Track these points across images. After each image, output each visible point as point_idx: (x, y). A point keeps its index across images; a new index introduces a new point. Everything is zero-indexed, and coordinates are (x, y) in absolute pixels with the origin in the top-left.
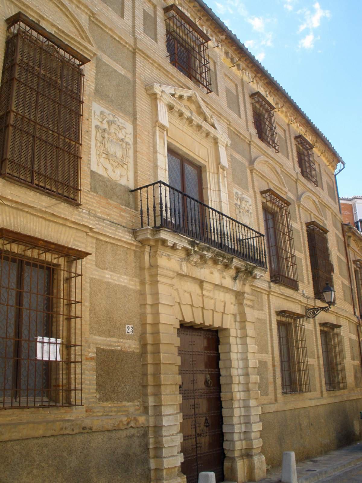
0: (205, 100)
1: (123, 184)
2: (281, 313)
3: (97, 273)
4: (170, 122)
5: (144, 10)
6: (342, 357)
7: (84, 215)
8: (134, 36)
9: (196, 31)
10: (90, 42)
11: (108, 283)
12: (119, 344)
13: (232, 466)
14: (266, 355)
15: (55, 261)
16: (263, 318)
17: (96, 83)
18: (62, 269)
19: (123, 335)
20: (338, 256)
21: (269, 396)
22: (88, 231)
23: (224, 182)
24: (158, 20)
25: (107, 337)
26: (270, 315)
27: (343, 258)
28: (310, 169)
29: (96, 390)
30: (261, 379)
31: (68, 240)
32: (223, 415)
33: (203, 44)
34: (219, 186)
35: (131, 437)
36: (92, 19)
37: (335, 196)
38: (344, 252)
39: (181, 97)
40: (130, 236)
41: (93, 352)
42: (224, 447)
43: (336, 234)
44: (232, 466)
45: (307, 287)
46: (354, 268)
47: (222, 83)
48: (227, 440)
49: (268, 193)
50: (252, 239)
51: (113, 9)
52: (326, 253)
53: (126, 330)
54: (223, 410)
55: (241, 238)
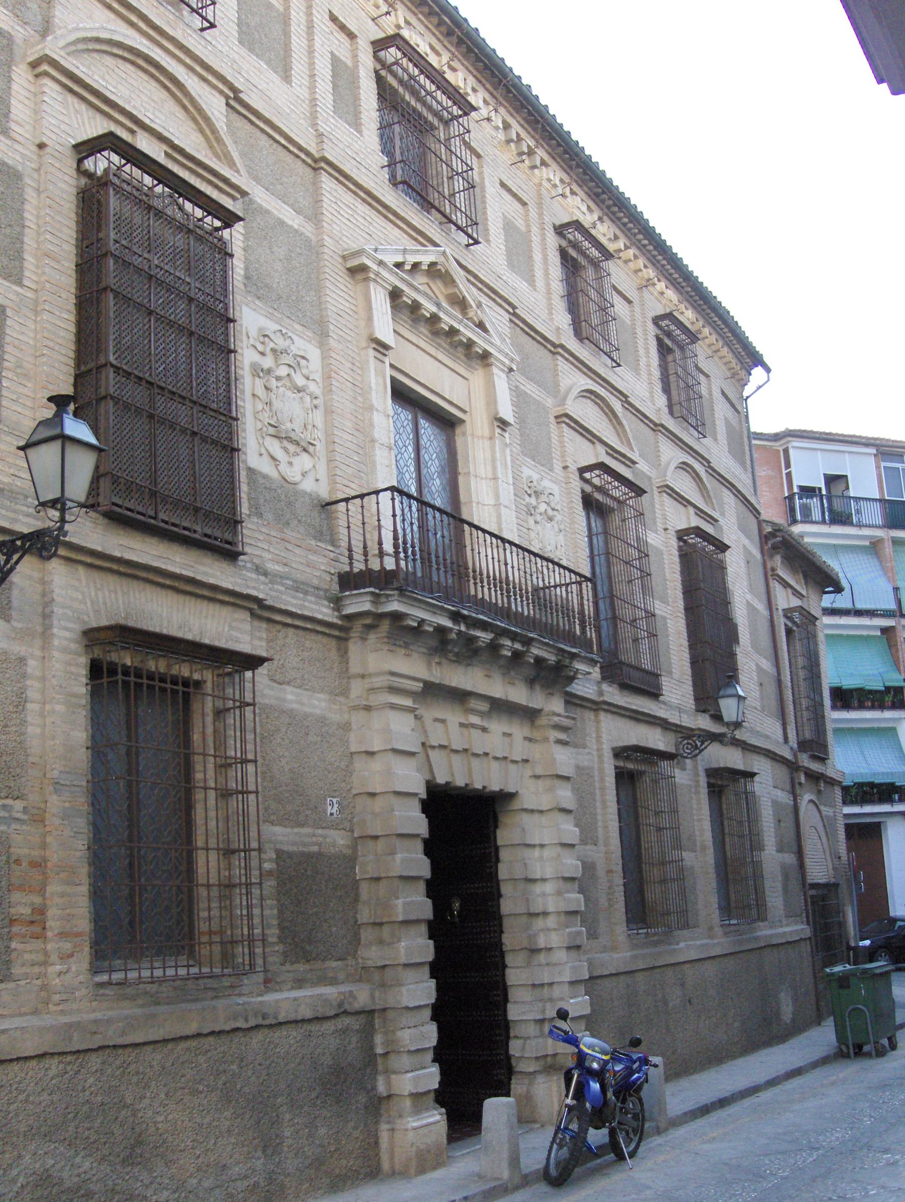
0: (464, 263)
1: (308, 490)
2: (620, 753)
3: (272, 693)
4: (395, 331)
5: (332, 53)
6: (757, 845)
7: (249, 574)
8: (314, 125)
9: (444, 93)
10: (232, 164)
11: (291, 714)
12: (314, 839)
13: (528, 1091)
14: (593, 847)
15: (196, 676)
16: (586, 763)
17: (246, 259)
18: (209, 691)
19: (322, 822)
20: (748, 602)
21: (601, 940)
22: (256, 607)
23: (505, 456)
24: (362, 73)
25: (293, 827)
26: (600, 757)
27: (761, 607)
28: (688, 395)
29: (279, 938)
30: (587, 900)
31: (220, 629)
32: (509, 983)
33: (457, 118)
34: (494, 468)
35: (344, 1031)
36: (232, 102)
37: (744, 453)
38: (762, 589)
39: (416, 266)
40: (329, 607)
41: (270, 860)
42: (511, 1052)
43: (744, 547)
44: (528, 1091)
45: (678, 694)
46: (786, 625)
47: (496, 208)
48: (516, 1037)
49: (597, 472)
50: (564, 588)
51: (268, 63)
52: (723, 601)
53: (325, 811)
54: (508, 971)
55: (541, 585)
